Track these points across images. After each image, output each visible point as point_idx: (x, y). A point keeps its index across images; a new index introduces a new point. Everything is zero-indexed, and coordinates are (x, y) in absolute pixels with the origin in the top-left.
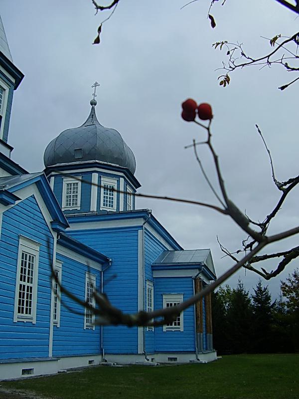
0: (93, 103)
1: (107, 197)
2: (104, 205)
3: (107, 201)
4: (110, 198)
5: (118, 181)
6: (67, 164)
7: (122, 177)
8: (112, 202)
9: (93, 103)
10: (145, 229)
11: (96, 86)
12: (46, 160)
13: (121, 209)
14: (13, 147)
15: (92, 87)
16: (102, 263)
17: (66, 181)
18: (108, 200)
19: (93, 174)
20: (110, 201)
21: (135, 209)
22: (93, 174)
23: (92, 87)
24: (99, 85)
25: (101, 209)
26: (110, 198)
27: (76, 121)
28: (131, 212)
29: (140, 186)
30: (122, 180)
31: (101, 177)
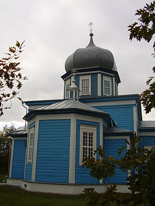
0: (91, 35)
1: (108, 87)
2: (105, 93)
3: (106, 90)
4: (108, 88)
5: (112, 79)
6: (90, 68)
7: (113, 76)
8: (109, 91)
9: (91, 35)
10: (68, 92)
11: (91, 25)
12: (66, 65)
13: (114, 95)
14: (149, 43)
15: (89, 25)
16: (108, 125)
17: (81, 78)
18: (107, 89)
19: (98, 74)
20: (106, 91)
21: (118, 95)
22: (98, 74)
23: (89, 25)
24: (93, 24)
25: (104, 95)
26: (108, 88)
27: (84, 44)
28: (114, 97)
29: (61, 77)
30: (114, 78)
31: (103, 76)
